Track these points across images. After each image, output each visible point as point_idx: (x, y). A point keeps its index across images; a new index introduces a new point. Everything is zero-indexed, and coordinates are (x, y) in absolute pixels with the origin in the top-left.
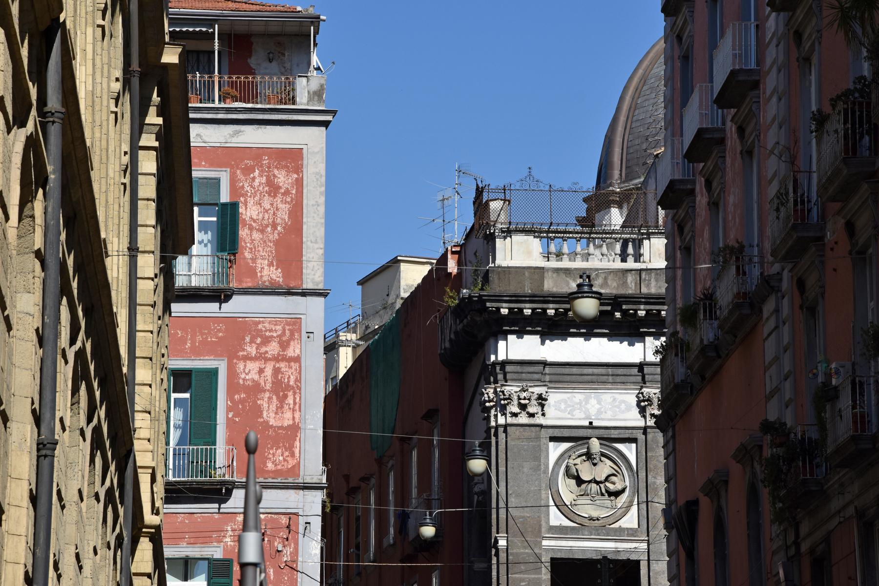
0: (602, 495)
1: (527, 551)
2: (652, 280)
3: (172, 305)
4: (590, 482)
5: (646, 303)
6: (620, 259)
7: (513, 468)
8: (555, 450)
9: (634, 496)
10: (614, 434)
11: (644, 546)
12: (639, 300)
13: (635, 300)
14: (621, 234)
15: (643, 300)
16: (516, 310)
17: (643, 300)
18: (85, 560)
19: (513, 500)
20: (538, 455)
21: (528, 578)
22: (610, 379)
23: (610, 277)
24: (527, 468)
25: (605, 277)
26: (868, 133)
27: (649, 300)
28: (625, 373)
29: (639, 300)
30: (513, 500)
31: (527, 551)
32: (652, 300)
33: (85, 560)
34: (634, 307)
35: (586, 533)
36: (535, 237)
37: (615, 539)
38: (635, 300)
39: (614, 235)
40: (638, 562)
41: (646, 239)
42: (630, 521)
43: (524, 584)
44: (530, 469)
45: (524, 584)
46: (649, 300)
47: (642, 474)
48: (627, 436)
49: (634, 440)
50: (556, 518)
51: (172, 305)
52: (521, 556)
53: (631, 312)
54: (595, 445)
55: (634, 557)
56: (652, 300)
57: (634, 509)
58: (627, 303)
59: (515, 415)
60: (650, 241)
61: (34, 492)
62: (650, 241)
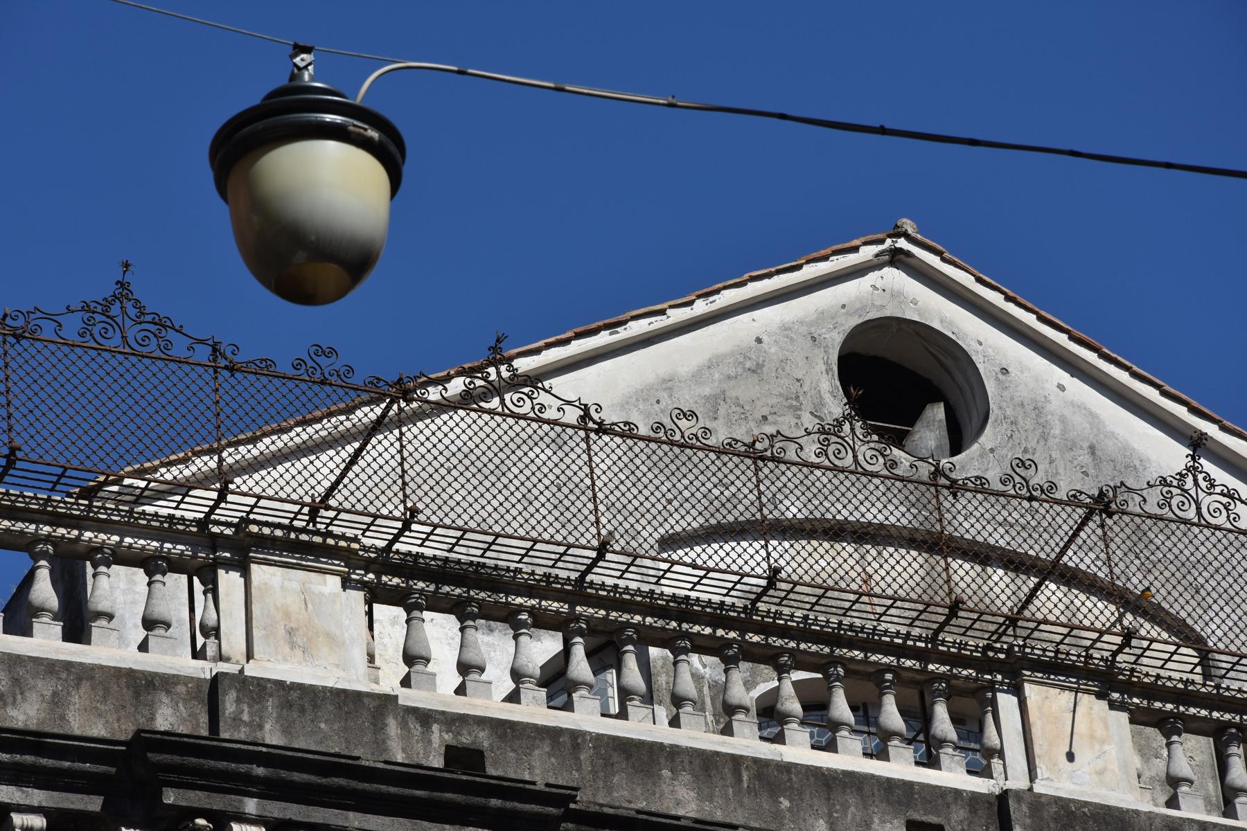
2: (268, 727)
5: (270, 790)
6: (57, 629)
12: (243, 768)
13: (223, 765)
14: (163, 540)
15: (260, 771)
17: (260, 771)
23: (75, 699)
25: (55, 694)
26: (746, 451)
27: (284, 774)
29: (243, 768)
32: (297, 777)
34: (218, 802)
36: (1113, 706)
38: (223, 765)
39: (88, 535)
41: (229, 566)
46: (284, 774)
53: (201, 822)
56: (297, 777)
58: (187, 779)
60: (246, 574)
61: (18, 692)
62: (246, 574)
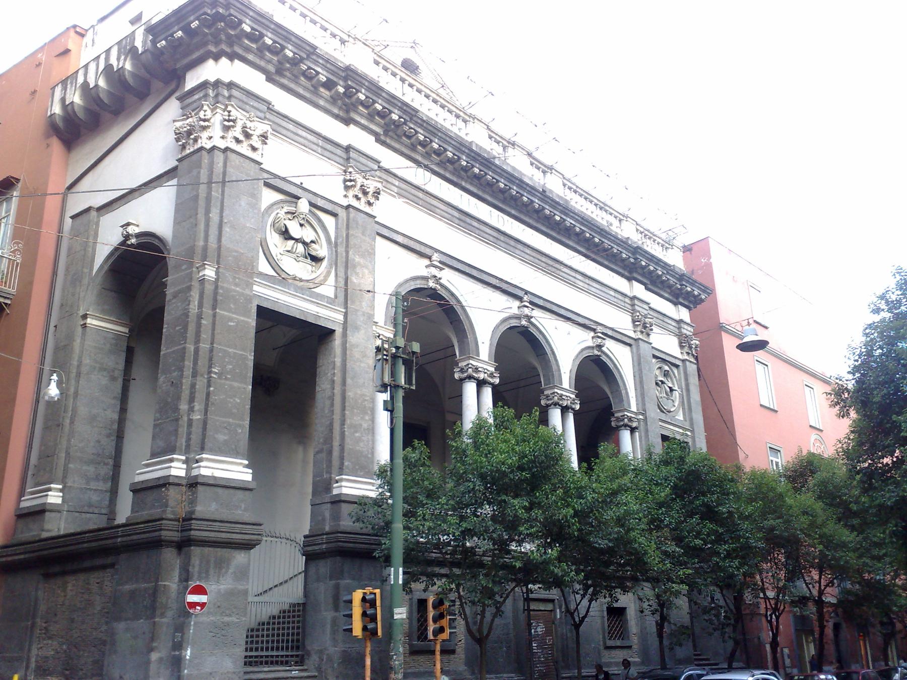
0: (306, 258)
1: (238, 289)
3: (60, 502)
4: (297, 240)
7: (230, 196)
8: (269, 197)
9: (331, 268)
10: (320, 203)
11: (341, 318)
16: (257, 33)
18: (121, 369)
19: (228, 230)
20: (255, 197)
21: (237, 319)
22: (319, 150)
24: (244, 202)
28: (332, 151)
30: (228, 230)
31: (238, 289)
33: (121, 369)
35: (292, 289)
37: (318, 303)
40: (332, 331)
42: (328, 290)
43: (232, 324)
44: (247, 204)
45: (232, 324)
47: (342, 249)
48: (330, 209)
49: (335, 215)
50: (264, 266)
51: (60, 502)
52: (231, 294)
54: (303, 206)
55: (330, 326)
57: (332, 279)
59: (238, 141)
